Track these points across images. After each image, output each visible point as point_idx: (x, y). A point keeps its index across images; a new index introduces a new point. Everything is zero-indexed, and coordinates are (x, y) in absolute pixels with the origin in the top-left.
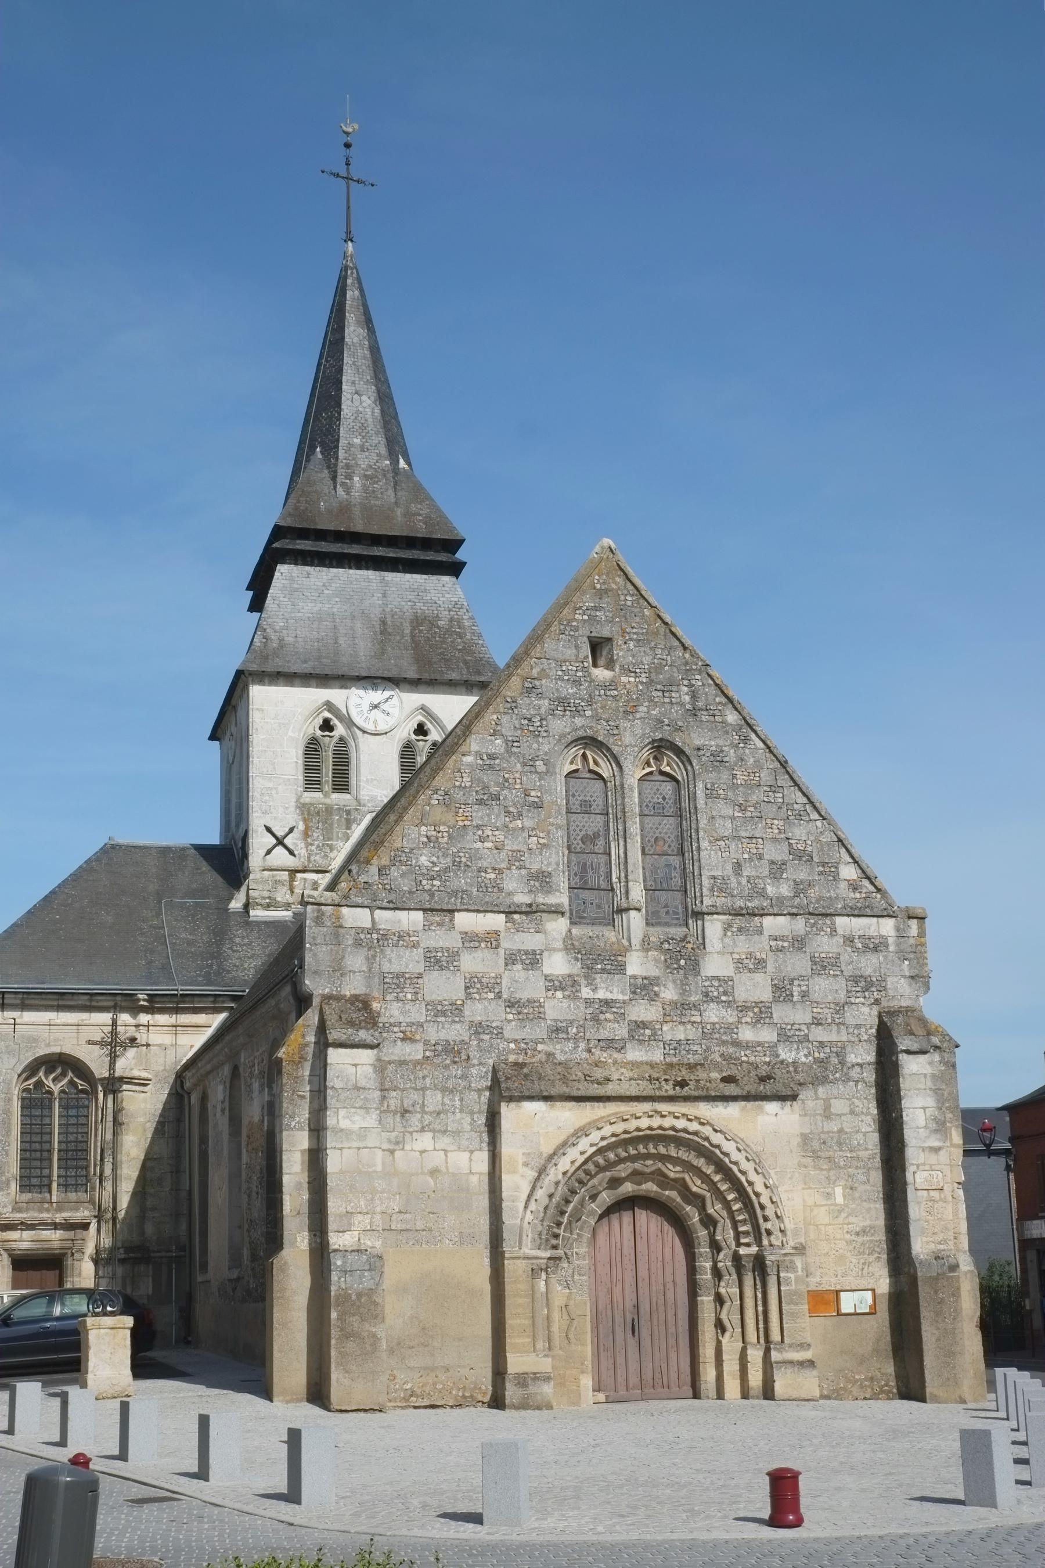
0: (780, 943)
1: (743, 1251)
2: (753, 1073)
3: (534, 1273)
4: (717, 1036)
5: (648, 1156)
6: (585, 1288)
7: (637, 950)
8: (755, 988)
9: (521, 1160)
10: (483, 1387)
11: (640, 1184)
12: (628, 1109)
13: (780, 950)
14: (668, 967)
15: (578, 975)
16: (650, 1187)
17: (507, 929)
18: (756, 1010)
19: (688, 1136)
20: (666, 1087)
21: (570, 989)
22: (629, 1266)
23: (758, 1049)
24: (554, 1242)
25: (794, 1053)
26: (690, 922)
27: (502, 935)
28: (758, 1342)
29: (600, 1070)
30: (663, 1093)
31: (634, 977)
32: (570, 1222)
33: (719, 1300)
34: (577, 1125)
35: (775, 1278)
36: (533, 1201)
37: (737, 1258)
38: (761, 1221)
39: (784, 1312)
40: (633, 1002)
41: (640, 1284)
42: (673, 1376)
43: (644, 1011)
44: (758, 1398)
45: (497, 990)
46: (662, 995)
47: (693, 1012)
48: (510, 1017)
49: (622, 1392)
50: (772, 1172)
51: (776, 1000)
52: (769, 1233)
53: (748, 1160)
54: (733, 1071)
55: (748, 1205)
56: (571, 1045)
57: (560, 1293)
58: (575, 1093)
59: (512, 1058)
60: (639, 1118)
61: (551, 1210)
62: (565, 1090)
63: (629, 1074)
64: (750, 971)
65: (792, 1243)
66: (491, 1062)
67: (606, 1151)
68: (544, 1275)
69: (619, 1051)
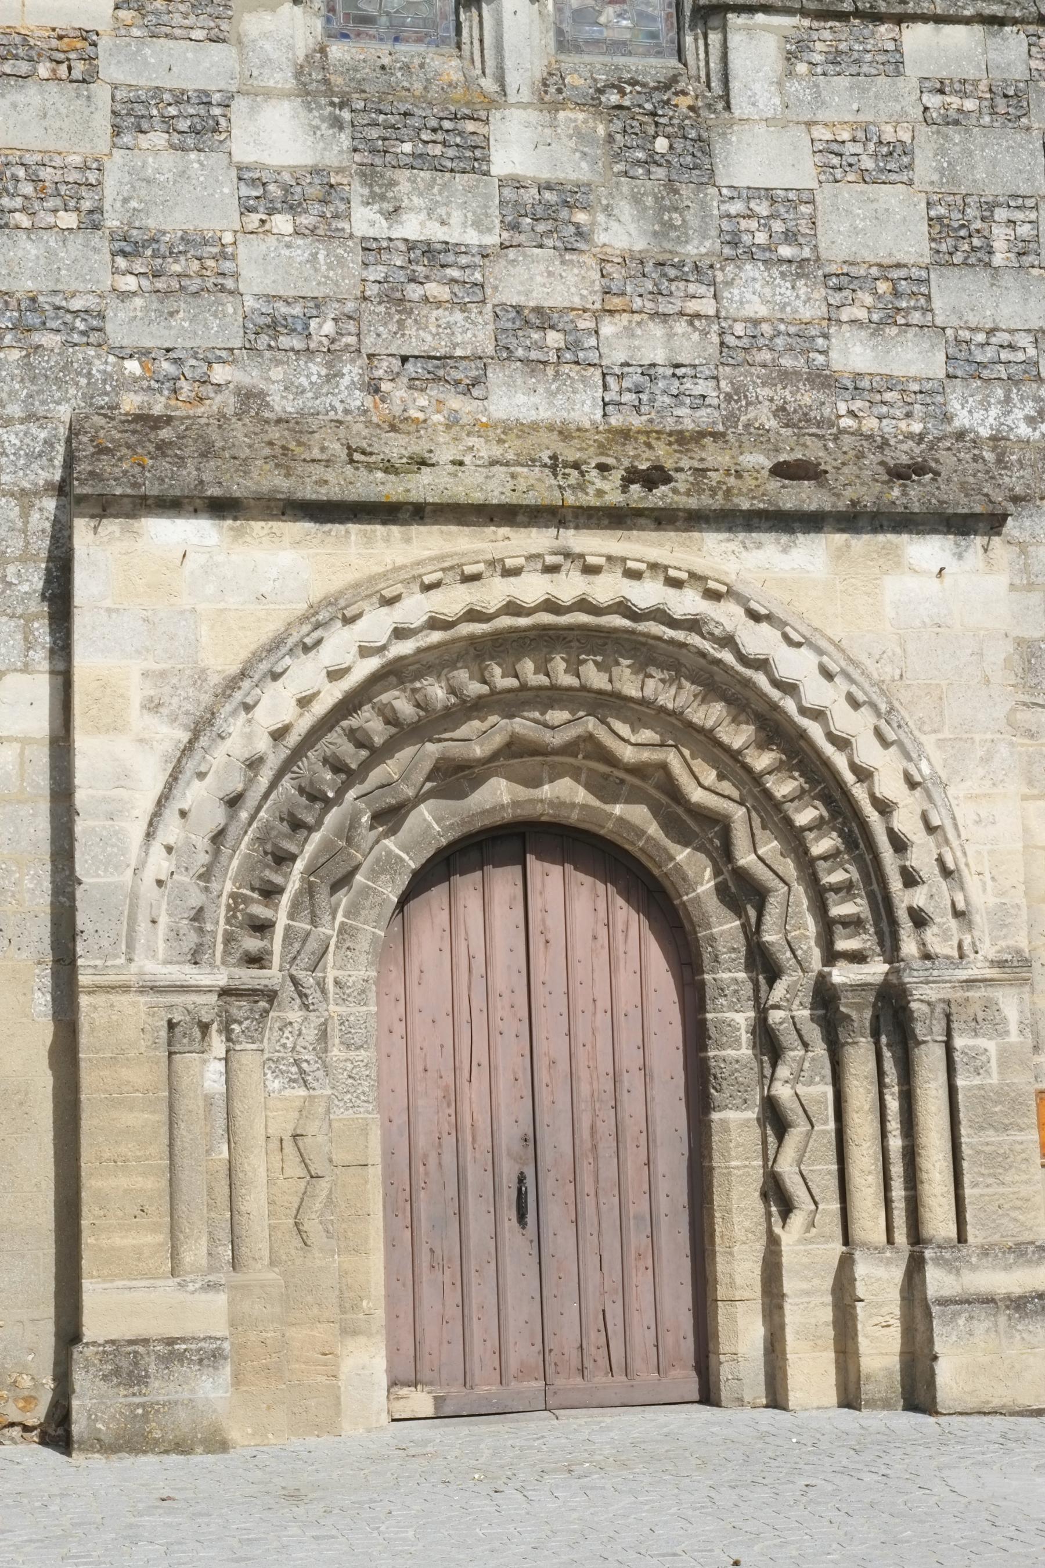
0: (955, 101)
1: (841, 974)
2: (871, 459)
3: (177, 1036)
4: (766, 356)
5: (552, 696)
6: (365, 1086)
7: (524, 106)
8: (884, 226)
9: (137, 692)
10: (26, 1381)
11: (535, 783)
12: (478, 545)
13: (954, 121)
14: (617, 157)
15: (340, 171)
16: (566, 794)
17: (120, 29)
18: (883, 287)
19: (669, 633)
20: (599, 484)
21: (316, 208)
22: (511, 1024)
23: (888, 396)
24: (252, 944)
25: (994, 412)
26: (689, 40)
27: (104, 42)
28: (890, 1241)
29: (402, 439)
30: (589, 499)
31: (518, 184)
32: (309, 890)
33: (775, 1119)
34: (318, 592)
35: (938, 1052)
36: (171, 814)
37: (825, 998)
38: (896, 884)
39: (966, 1151)
40: (512, 253)
41: (543, 1075)
42: (642, 1337)
43: (537, 279)
44: (887, 1405)
45: (86, 205)
46: (601, 238)
47: (692, 288)
48: (130, 283)
49: (487, 1388)
50: (929, 742)
51: (943, 262)
52: (920, 919)
53: (855, 704)
54: (813, 451)
55: (858, 841)
56: (316, 369)
57: (272, 1102)
58: (309, 492)
59: (130, 403)
60: (516, 572)
61: (242, 850)
62: (278, 483)
63: (486, 450)
64: (864, 176)
65: (988, 950)
66: (64, 412)
67: (419, 676)
68: (218, 1044)
69: (468, 388)
